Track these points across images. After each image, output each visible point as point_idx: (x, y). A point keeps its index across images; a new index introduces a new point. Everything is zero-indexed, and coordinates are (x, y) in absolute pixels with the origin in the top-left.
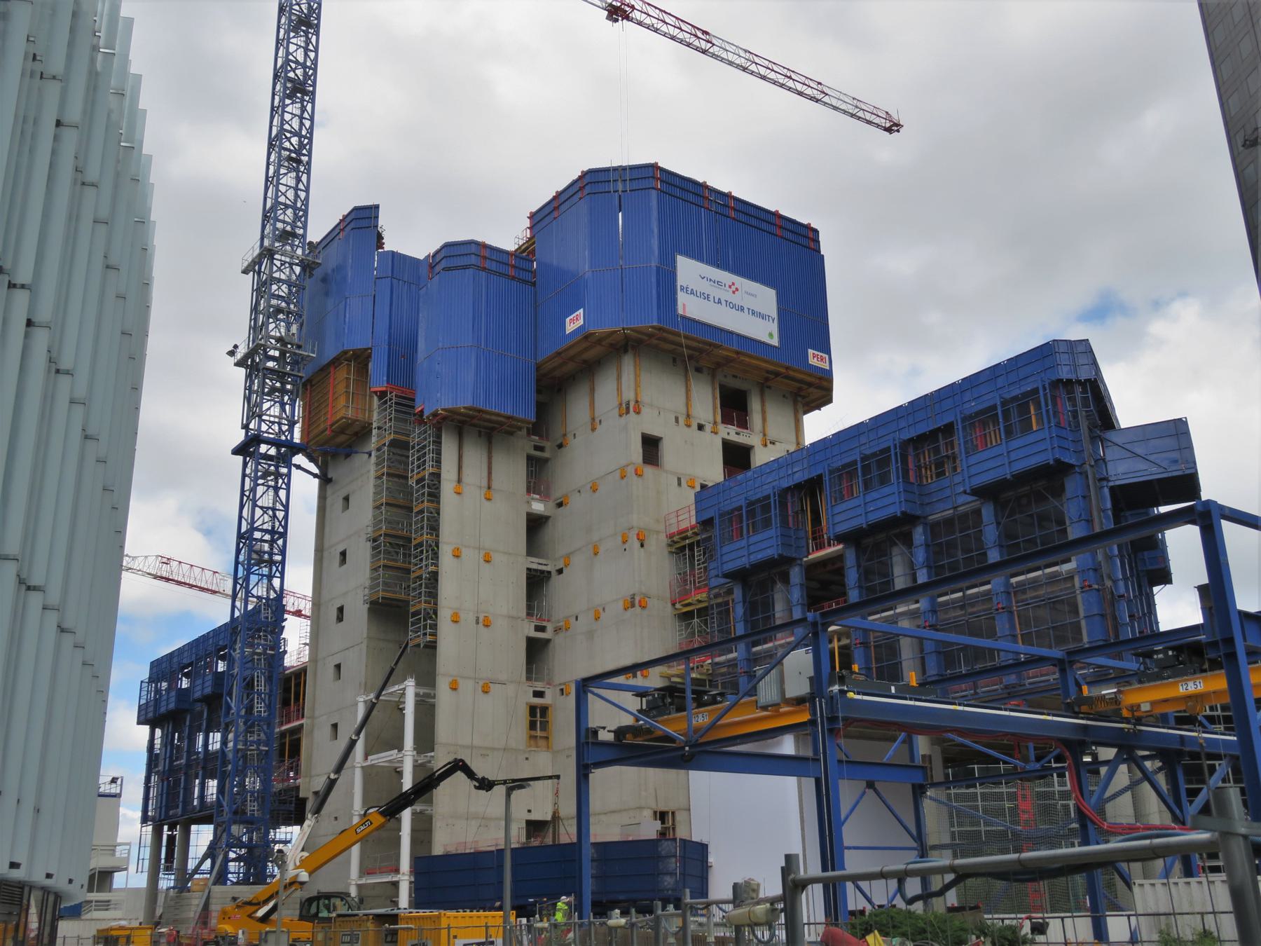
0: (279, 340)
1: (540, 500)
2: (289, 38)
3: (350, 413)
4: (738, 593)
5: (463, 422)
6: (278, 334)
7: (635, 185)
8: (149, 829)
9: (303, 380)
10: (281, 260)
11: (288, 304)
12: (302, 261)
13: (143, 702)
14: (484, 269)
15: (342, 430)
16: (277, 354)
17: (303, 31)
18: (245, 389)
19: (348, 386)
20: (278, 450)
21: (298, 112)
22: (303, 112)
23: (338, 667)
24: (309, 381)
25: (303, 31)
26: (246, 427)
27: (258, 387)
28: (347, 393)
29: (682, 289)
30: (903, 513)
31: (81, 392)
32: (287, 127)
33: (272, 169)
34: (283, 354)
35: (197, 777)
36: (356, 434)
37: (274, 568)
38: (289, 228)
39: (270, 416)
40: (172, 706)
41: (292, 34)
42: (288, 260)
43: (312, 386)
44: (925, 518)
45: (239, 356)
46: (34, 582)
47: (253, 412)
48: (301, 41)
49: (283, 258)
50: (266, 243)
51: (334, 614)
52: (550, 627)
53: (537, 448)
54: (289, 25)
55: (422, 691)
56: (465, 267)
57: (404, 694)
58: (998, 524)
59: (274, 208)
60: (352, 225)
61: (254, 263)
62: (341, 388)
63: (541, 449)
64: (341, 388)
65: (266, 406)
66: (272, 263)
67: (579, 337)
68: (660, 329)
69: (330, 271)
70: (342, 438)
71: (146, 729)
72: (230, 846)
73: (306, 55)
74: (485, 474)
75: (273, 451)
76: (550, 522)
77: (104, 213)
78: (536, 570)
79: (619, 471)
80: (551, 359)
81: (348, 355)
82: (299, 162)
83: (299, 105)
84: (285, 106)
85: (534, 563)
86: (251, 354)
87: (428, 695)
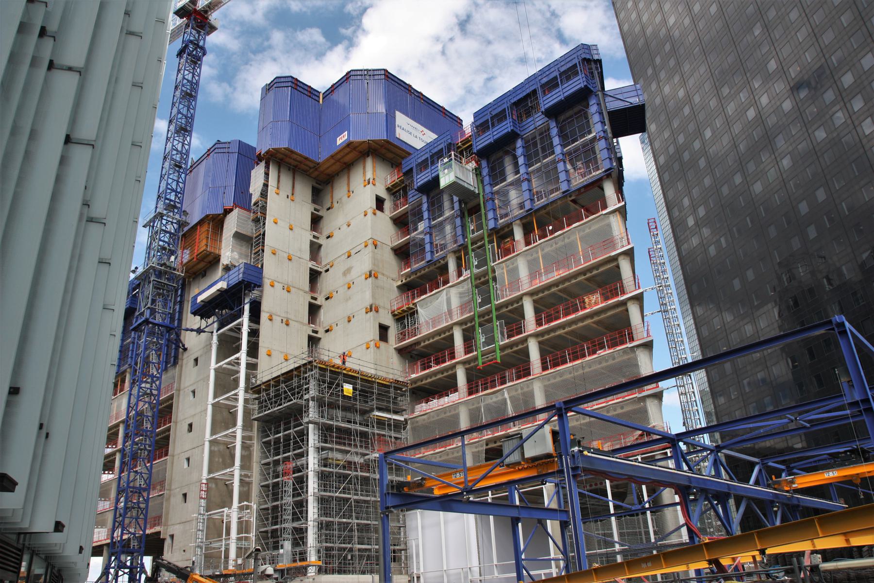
4: (424, 199)
5: (282, 160)
36: (210, 262)
37: (153, 398)
38: (172, 203)
42: (171, 220)
49: (168, 219)
51: (186, 427)
61: (150, 221)
63: (316, 332)
64: (204, 236)
67: (344, 145)
68: (387, 142)
80: (327, 160)
82: (180, 167)
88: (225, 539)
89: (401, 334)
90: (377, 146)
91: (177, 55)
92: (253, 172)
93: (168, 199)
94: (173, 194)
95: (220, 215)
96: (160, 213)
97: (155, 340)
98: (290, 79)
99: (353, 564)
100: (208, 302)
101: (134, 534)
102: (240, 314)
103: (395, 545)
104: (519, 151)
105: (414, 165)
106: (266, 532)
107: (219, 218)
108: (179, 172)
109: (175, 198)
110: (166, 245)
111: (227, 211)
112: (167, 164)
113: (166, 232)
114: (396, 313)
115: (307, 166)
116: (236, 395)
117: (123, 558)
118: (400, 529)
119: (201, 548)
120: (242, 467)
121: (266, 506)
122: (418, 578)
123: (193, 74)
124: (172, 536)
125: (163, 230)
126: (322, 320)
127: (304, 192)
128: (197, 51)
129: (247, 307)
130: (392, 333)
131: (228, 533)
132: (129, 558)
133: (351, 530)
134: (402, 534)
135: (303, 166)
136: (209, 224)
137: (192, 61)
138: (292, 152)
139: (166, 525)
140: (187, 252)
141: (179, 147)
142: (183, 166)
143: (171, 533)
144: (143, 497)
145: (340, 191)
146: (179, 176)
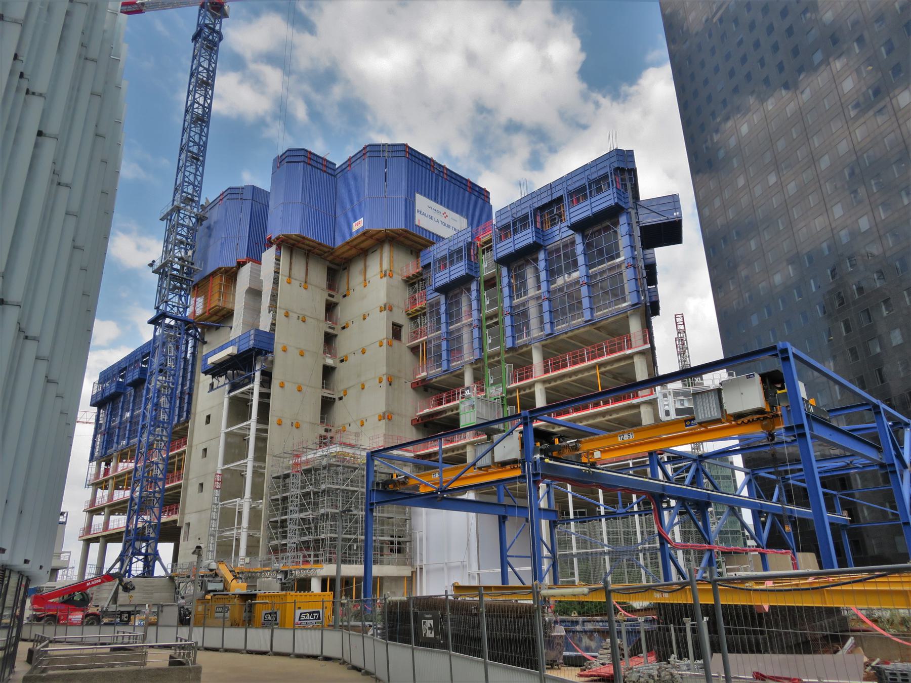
0: (180, 259)
1: (331, 358)
2: (191, 128)
3: (221, 304)
5: (293, 245)
6: (180, 255)
7: (395, 154)
8: (95, 463)
9: (194, 283)
10: (184, 214)
11: (187, 239)
12: (196, 215)
13: (95, 392)
14: (310, 164)
15: (216, 313)
16: (178, 267)
17: (200, 124)
18: (158, 286)
19: (220, 288)
20: (176, 322)
21: (194, 171)
22: (196, 171)
23: (205, 450)
24: (197, 284)
25: (200, 124)
26: (157, 308)
27: (166, 285)
28: (220, 292)
29: (418, 212)
30: (534, 242)
31: (45, 351)
32: (186, 179)
33: (186, 124)
34: (182, 267)
35: (128, 411)
36: (223, 316)
38: (189, 196)
39: (173, 302)
40: (113, 391)
41: (193, 126)
42: (188, 214)
43: (198, 288)
44: (545, 247)
45: (155, 267)
46: (31, 333)
47: (162, 299)
48: (198, 130)
49: (186, 213)
50: (175, 203)
52: (333, 430)
53: (330, 328)
54: (191, 120)
55: (257, 465)
56: (298, 162)
57: (253, 390)
58: (584, 244)
59: (182, 185)
60: (228, 197)
61: (168, 214)
62: (216, 289)
65: (170, 297)
66: (179, 216)
67: (360, 233)
68: (406, 231)
69: (212, 224)
70: (215, 318)
71: (95, 409)
72: (134, 554)
73: (200, 138)
74: (304, 275)
75: (173, 323)
76: (337, 370)
77: (75, 207)
78: (327, 397)
79: (378, 343)
80: (343, 246)
81: (222, 270)
82: (198, 160)
83: (194, 167)
84: (186, 167)
85: (327, 393)
86: (163, 266)
87: (260, 467)
88: (237, 528)
89: (414, 333)
90: (395, 235)
91: (193, 40)
92: (264, 255)
93: (185, 192)
94: (191, 187)
95: (233, 268)
96: (178, 207)
97: (172, 334)
98: (303, 153)
99: (357, 554)
100: (218, 364)
101: (150, 522)
102: (251, 380)
103: (399, 537)
104: (542, 265)
105: (431, 260)
106: (276, 522)
107: (233, 270)
108: (196, 165)
109: (193, 192)
110: (184, 239)
111: (241, 264)
112: (183, 156)
113: (183, 225)
114: (409, 312)
115: (321, 250)
116: (249, 425)
117: (137, 544)
118: (405, 522)
119: (214, 536)
120: (256, 459)
121: (276, 497)
122: (421, 569)
123: (210, 61)
124: (188, 524)
125: (180, 224)
126: (339, 317)
127: (319, 275)
128: (213, 36)
129: (258, 375)
130: (405, 332)
131: (240, 523)
132: (144, 544)
133: (356, 522)
134: (408, 526)
135: (316, 251)
136: (221, 276)
137: (207, 46)
138: (304, 238)
139: (183, 514)
140: (200, 300)
141: (197, 139)
142: (201, 158)
143: (187, 522)
144: (159, 487)
145: (355, 276)
146: (197, 169)
